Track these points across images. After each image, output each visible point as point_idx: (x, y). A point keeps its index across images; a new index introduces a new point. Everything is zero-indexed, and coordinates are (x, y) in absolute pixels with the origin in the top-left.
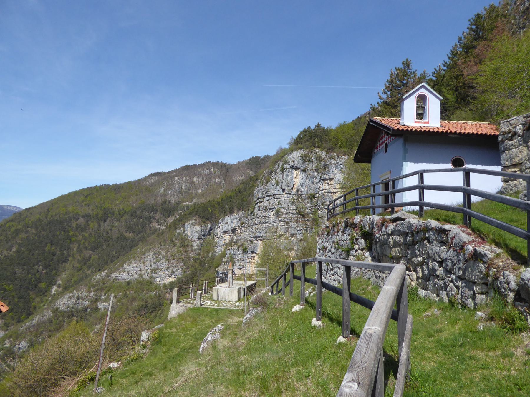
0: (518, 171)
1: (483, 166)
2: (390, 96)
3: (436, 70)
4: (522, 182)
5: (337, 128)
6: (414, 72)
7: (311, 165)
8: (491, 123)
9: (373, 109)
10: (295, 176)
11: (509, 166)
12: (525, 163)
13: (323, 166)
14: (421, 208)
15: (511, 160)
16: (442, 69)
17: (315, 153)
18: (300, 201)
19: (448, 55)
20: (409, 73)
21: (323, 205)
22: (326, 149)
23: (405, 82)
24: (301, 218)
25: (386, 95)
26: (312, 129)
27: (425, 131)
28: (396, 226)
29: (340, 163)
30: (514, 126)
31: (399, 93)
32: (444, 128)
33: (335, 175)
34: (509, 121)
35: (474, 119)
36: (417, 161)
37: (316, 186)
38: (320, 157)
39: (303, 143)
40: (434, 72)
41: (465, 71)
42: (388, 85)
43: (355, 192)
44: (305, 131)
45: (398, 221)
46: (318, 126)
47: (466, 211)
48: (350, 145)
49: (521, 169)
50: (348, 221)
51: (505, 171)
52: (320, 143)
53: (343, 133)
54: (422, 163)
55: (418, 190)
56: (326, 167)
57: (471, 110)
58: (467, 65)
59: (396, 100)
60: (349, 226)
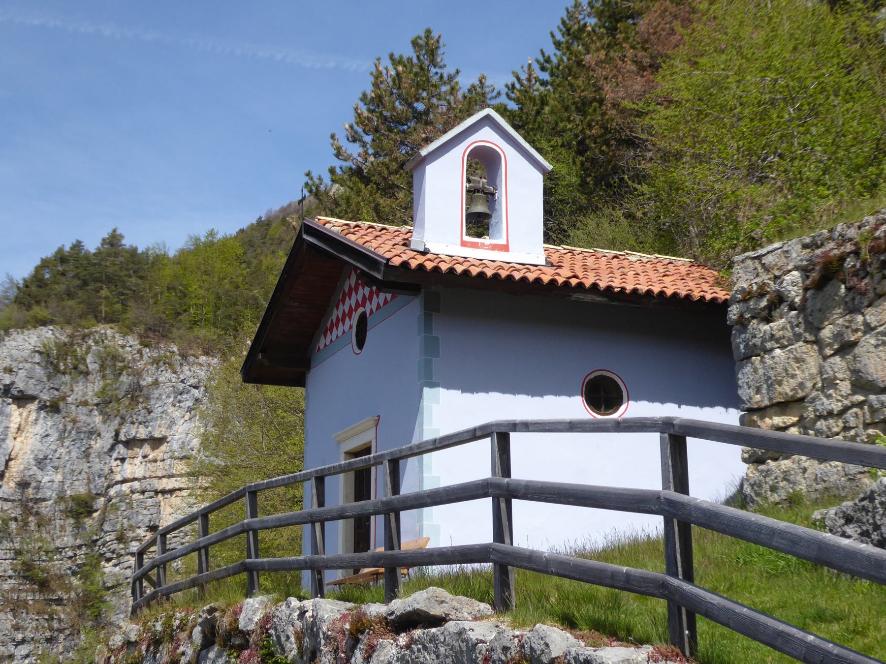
0: (793, 425)
1: (683, 407)
2: (371, 151)
3: (518, 79)
4: (806, 465)
5: (182, 252)
6: (451, 78)
7: (79, 388)
8: (697, 262)
9: (315, 191)
10: (14, 426)
11: (766, 408)
12: (814, 400)
13: (127, 393)
14: (502, 570)
15: (769, 387)
16: (537, 79)
17: (97, 343)
18: (33, 526)
19: (553, 36)
20: (435, 79)
21: (121, 539)
22: (141, 329)
23: (420, 106)
24: (33, 591)
25: (357, 144)
26: (87, 253)
27: (496, 276)
28: (408, 647)
29: (192, 381)
30: (777, 273)
31: (402, 143)
32: (559, 271)
33: (170, 427)
34: (759, 258)
35: (640, 246)
36: (470, 386)
37: (97, 466)
38: (115, 358)
39: (53, 303)
40: (513, 85)
41: (607, 88)
42: (366, 114)
43: (246, 500)
44: (61, 258)
45: (415, 628)
46: (113, 241)
47: (677, 589)
48: (229, 317)
49: (802, 418)
50: (214, 619)
51: (754, 424)
52: (118, 306)
53: (206, 273)
54: (487, 392)
55: (489, 500)
56: (137, 394)
57: (629, 216)
58: (615, 72)
59: (394, 166)
60: (217, 640)
